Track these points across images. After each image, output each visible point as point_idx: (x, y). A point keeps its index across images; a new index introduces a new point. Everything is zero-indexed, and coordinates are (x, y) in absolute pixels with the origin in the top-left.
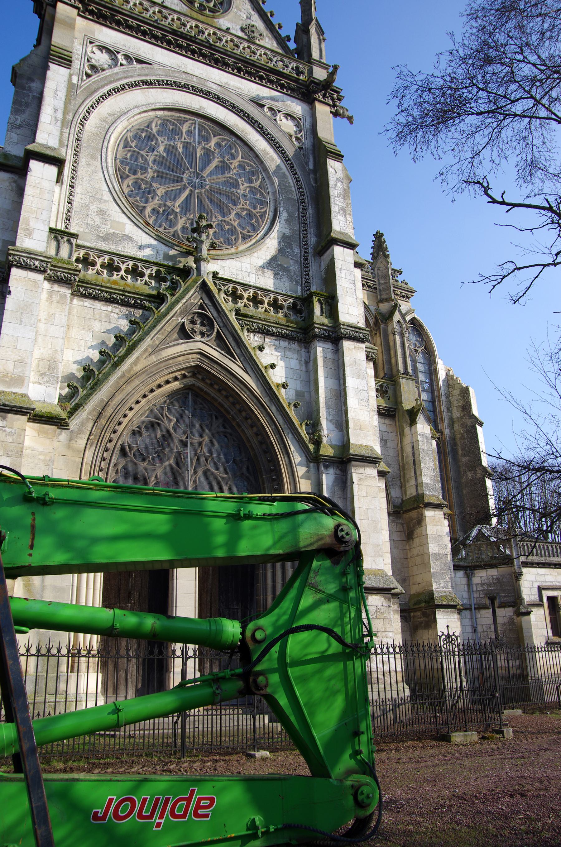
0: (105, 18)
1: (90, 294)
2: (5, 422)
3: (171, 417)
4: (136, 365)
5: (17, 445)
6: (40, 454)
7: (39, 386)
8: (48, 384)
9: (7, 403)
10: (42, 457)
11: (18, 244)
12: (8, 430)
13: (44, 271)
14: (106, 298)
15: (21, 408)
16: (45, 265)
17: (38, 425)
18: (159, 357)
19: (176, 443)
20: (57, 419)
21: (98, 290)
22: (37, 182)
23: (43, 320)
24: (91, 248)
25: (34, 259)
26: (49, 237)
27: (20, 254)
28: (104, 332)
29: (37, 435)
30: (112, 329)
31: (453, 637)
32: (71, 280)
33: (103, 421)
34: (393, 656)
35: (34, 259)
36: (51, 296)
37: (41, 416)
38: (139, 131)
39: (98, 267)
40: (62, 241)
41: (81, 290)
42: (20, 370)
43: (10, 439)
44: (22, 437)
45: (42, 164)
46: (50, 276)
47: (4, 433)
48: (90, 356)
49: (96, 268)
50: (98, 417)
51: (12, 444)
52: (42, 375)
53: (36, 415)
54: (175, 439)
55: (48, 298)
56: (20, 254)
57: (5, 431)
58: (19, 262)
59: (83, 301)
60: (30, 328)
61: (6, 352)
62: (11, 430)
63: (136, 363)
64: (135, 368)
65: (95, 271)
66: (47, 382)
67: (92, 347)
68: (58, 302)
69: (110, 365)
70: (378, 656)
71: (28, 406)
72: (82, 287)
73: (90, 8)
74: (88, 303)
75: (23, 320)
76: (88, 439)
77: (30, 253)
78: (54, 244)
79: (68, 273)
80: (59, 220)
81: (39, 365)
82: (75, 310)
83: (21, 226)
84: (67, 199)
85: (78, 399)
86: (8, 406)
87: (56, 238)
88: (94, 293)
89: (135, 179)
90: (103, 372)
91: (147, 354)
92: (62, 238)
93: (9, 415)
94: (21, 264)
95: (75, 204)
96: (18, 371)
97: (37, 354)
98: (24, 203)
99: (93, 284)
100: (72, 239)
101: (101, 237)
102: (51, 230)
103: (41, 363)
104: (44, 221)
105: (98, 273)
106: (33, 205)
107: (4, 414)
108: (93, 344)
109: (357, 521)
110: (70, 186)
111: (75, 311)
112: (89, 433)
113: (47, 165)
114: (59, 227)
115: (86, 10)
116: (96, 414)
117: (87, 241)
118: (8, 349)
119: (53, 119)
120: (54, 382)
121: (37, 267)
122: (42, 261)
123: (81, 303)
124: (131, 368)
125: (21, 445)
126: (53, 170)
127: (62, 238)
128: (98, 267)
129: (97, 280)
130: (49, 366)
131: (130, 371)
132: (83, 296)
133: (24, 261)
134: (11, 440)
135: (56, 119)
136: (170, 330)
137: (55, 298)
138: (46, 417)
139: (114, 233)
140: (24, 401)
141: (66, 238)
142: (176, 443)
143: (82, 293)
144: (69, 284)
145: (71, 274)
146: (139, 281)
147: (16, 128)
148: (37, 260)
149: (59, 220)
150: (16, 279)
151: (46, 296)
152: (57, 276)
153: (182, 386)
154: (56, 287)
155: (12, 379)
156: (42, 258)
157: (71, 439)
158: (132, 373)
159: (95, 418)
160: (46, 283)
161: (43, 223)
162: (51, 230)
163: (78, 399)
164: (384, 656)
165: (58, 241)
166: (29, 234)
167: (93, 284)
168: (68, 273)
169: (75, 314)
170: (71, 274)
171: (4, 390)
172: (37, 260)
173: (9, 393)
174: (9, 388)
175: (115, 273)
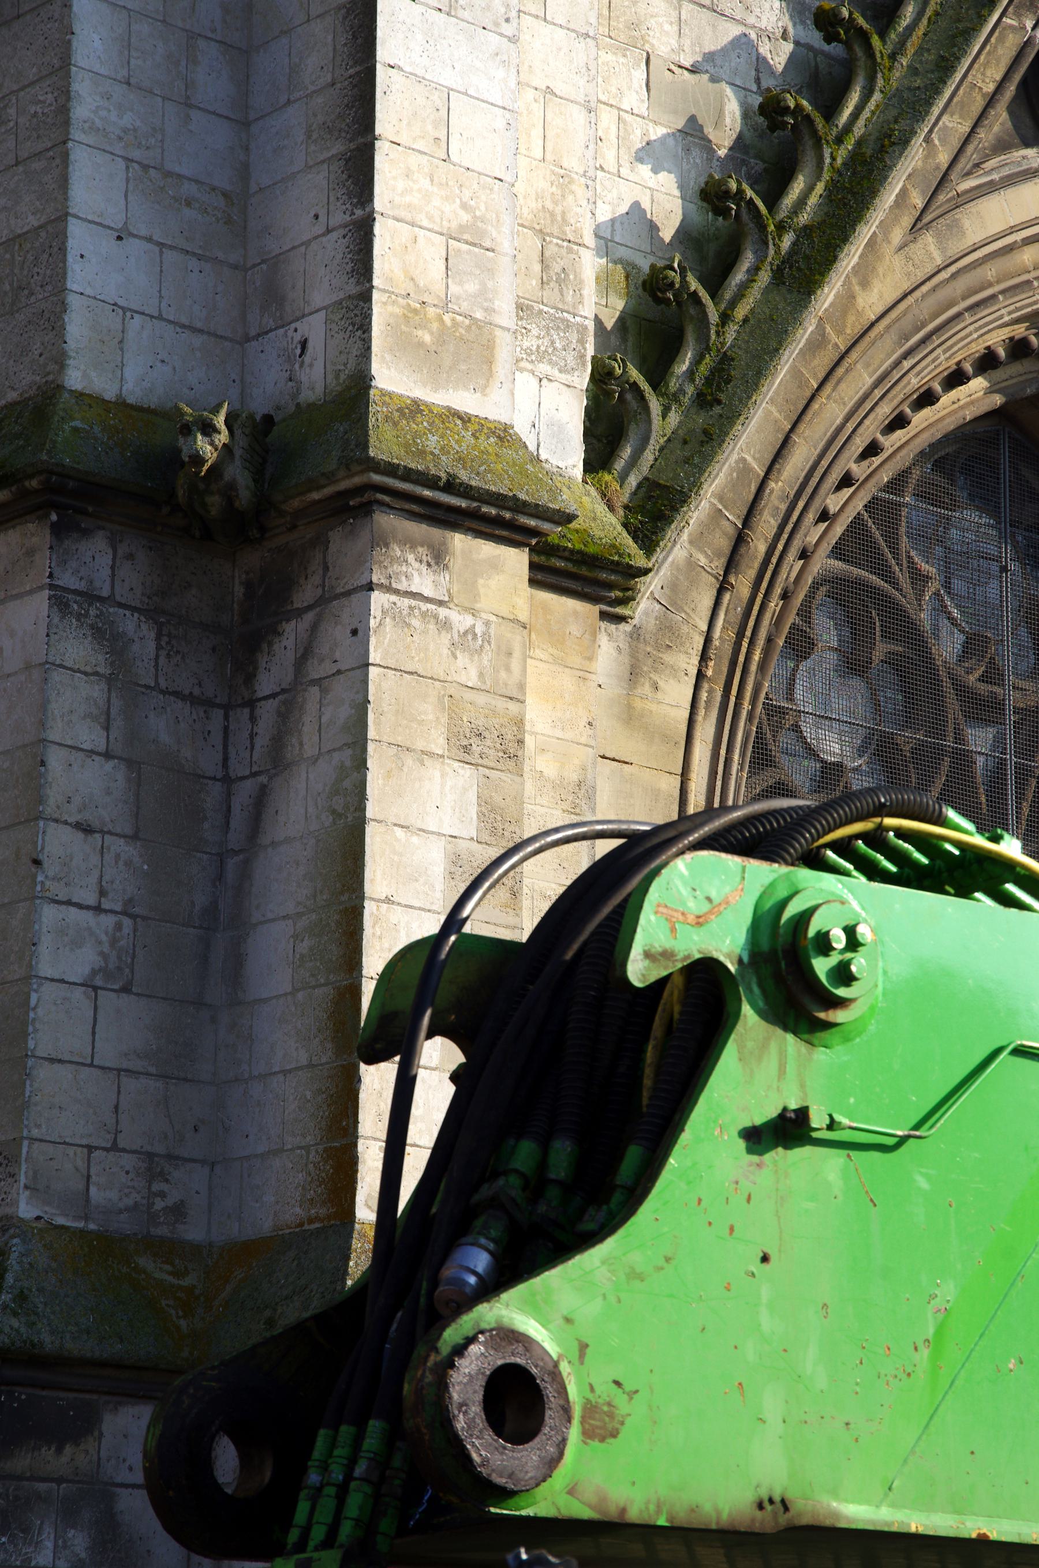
2: (444, 578)
3: (925, 567)
4: (865, 284)
8: (544, 368)
12: (461, 621)
18: (956, 247)
19: (953, 706)
28: (693, 70)
30: (724, 51)
33: (743, 584)
47: (445, 639)
48: (646, 205)
50: (732, 564)
51: (481, 699)
54: (947, 684)
57: (445, 625)
62: (468, 621)
63: (864, 275)
64: (861, 302)
66: (542, 356)
67: (647, 153)
69: (764, 277)
76: (700, 676)
85: (649, 456)
90: (741, 312)
91: (907, 221)
93: (459, 541)
107: (436, 533)
108: (657, 132)
109: (704, 853)
112: (699, 642)
116: (725, 544)
118: (414, 159)
124: (848, 299)
125: (513, 707)
131: (844, 313)
134: (473, 680)
136: (991, 88)
142: (953, 706)
153: (998, 400)
155: (443, 335)
157: (634, 674)
158: (852, 327)
159: (718, 565)
163: (649, 456)
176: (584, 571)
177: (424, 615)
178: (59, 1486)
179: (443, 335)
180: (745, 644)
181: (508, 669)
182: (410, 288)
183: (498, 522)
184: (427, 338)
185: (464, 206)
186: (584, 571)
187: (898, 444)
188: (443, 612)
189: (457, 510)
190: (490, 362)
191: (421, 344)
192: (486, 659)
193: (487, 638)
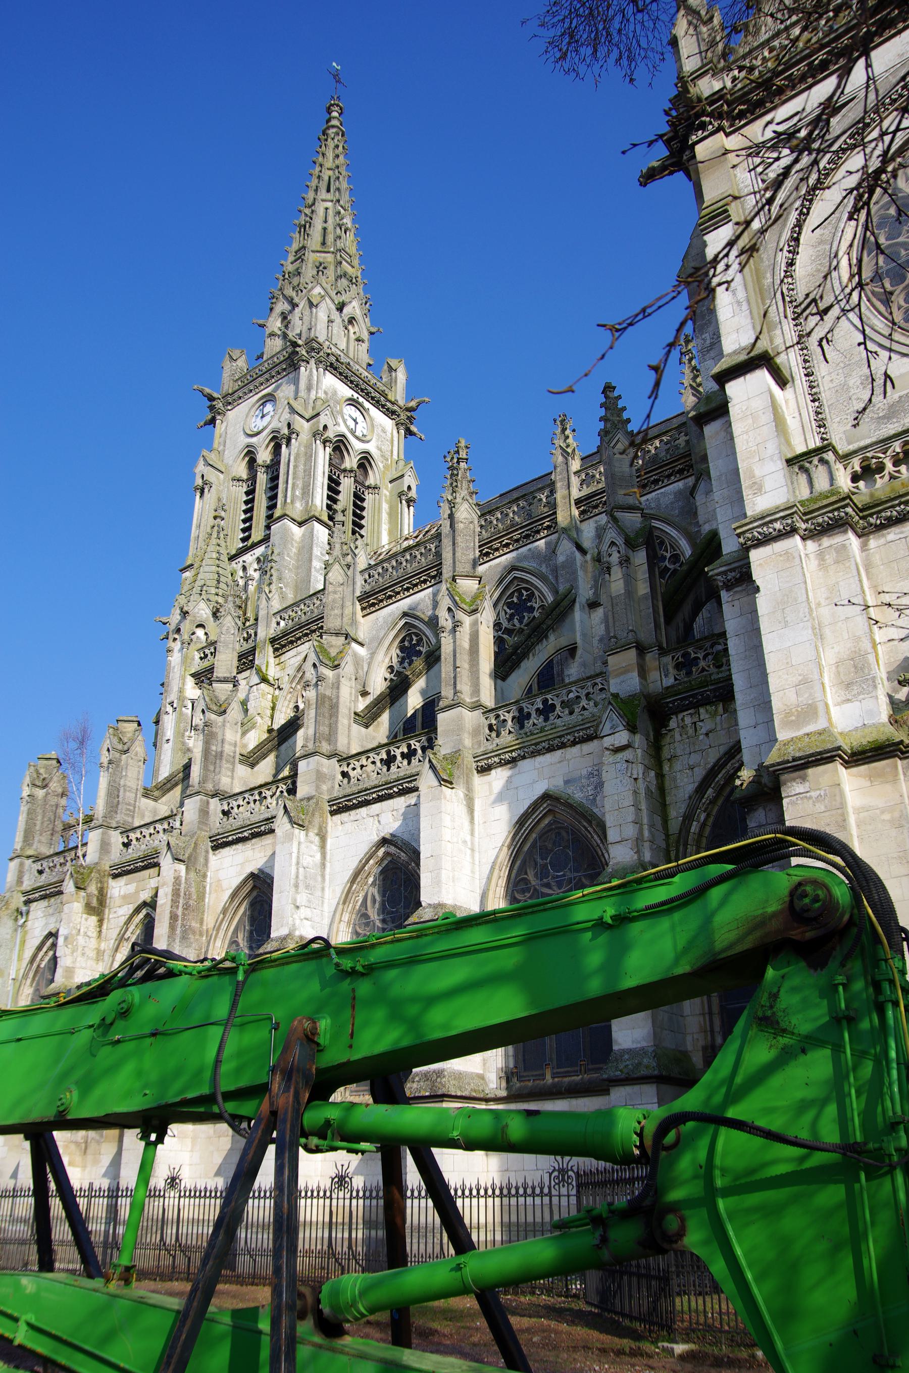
0: (760, 103)
1: (889, 519)
2: (807, 784)
5: (834, 812)
6: (883, 812)
7: (849, 705)
8: (862, 696)
9: (798, 755)
10: (887, 817)
11: (749, 513)
12: (814, 794)
13: (793, 531)
14: (736, 579)
15: (820, 753)
16: (789, 521)
17: (866, 766)
20: (889, 746)
21: (899, 505)
22: (744, 408)
23: (823, 603)
24: (866, 447)
25: (771, 522)
26: (791, 473)
27: (751, 526)
29: (868, 784)
31: (347, 1179)
32: (842, 518)
34: (523, 1199)
35: (771, 522)
36: (823, 560)
37: (863, 752)
38: (882, 212)
39: (889, 466)
40: (812, 469)
41: (872, 520)
42: (806, 696)
43: (821, 807)
44: (838, 798)
45: (741, 379)
46: (811, 531)
47: (811, 801)
49: (886, 472)
51: (827, 814)
52: (848, 686)
53: (854, 754)
55: (819, 565)
56: (751, 526)
57: (811, 797)
58: (753, 539)
59: (883, 536)
60: (801, 625)
61: (780, 677)
62: (818, 792)
65: (887, 478)
66: (859, 694)
68: (837, 562)
70: (473, 1199)
71: (829, 746)
72: (871, 515)
73: (736, 111)
74: (892, 534)
75: (788, 619)
77: (763, 518)
78: (803, 478)
79: (832, 511)
80: (809, 435)
81: (839, 673)
82: (877, 557)
83: (745, 483)
84: (809, 398)
86: (800, 758)
87: (801, 468)
88: (895, 513)
89: (904, 288)
92: (810, 462)
93: (810, 771)
94: (758, 539)
95: (823, 397)
96: (804, 699)
97: (829, 657)
98: (737, 450)
99: (886, 502)
100: (824, 455)
101: (884, 417)
102: (790, 462)
103: (841, 669)
104: (771, 457)
105: (892, 477)
106: (750, 444)
107: (801, 773)
110: (806, 375)
111: (876, 559)
113: (748, 376)
114: (812, 446)
115: (733, 119)
117: (863, 438)
119: (735, 306)
120: (871, 689)
121: (779, 531)
122: (783, 518)
123: (882, 541)
125: (839, 811)
126: (763, 376)
127: (810, 462)
128: (889, 466)
129: (893, 490)
130: (855, 667)
132: (881, 527)
133: (759, 533)
134: (823, 808)
135: (739, 303)
137: (830, 558)
138: (871, 750)
139: (900, 397)
140: (823, 741)
141: (815, 460)
143: (876, 526)
144: (843, 525)
145: (838, 509)
146: (879, 480)
147: (708, 351)
148: (776, 520)
149: (809, 435)
150: (761, 565)
151: (816, 562)
152: (819, 525)
154: (826, 541)
156: (782, 514)
160: (809, 543)
161: (772, 460)
162: (790, 462)
164: (528, 1198)
165: (806, 471)
166: (759, 488)
167: (886, 502)
168: (832, 511)
169: (879, 563)
170: (838, 509)
171: (794, 735)
172: (776, 520)
173: (800, 739)
174: (799, 729)
175: (877, 476)
176: (880, 752)
177: (802, 798)
178: (303, 1342)
179: (798, 716)
180: (530, 910)
181: (835, 800)
182: (785, 707)
183: (817, 760)
184: (794, 718)
185: (800, 675)
186: (880, 752)
187: (350, 895)
188: (808, 795)
189: (802, 764)
190: (816, 713)
191: (792, 721)
192: (826, 801)
193: (826, 795)
